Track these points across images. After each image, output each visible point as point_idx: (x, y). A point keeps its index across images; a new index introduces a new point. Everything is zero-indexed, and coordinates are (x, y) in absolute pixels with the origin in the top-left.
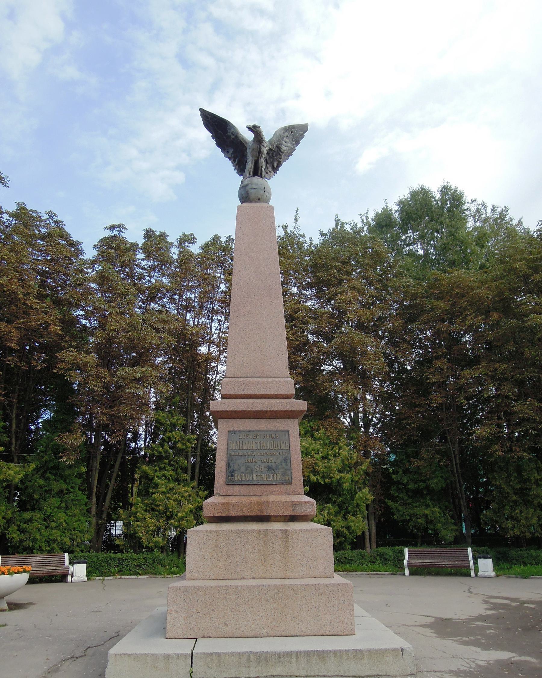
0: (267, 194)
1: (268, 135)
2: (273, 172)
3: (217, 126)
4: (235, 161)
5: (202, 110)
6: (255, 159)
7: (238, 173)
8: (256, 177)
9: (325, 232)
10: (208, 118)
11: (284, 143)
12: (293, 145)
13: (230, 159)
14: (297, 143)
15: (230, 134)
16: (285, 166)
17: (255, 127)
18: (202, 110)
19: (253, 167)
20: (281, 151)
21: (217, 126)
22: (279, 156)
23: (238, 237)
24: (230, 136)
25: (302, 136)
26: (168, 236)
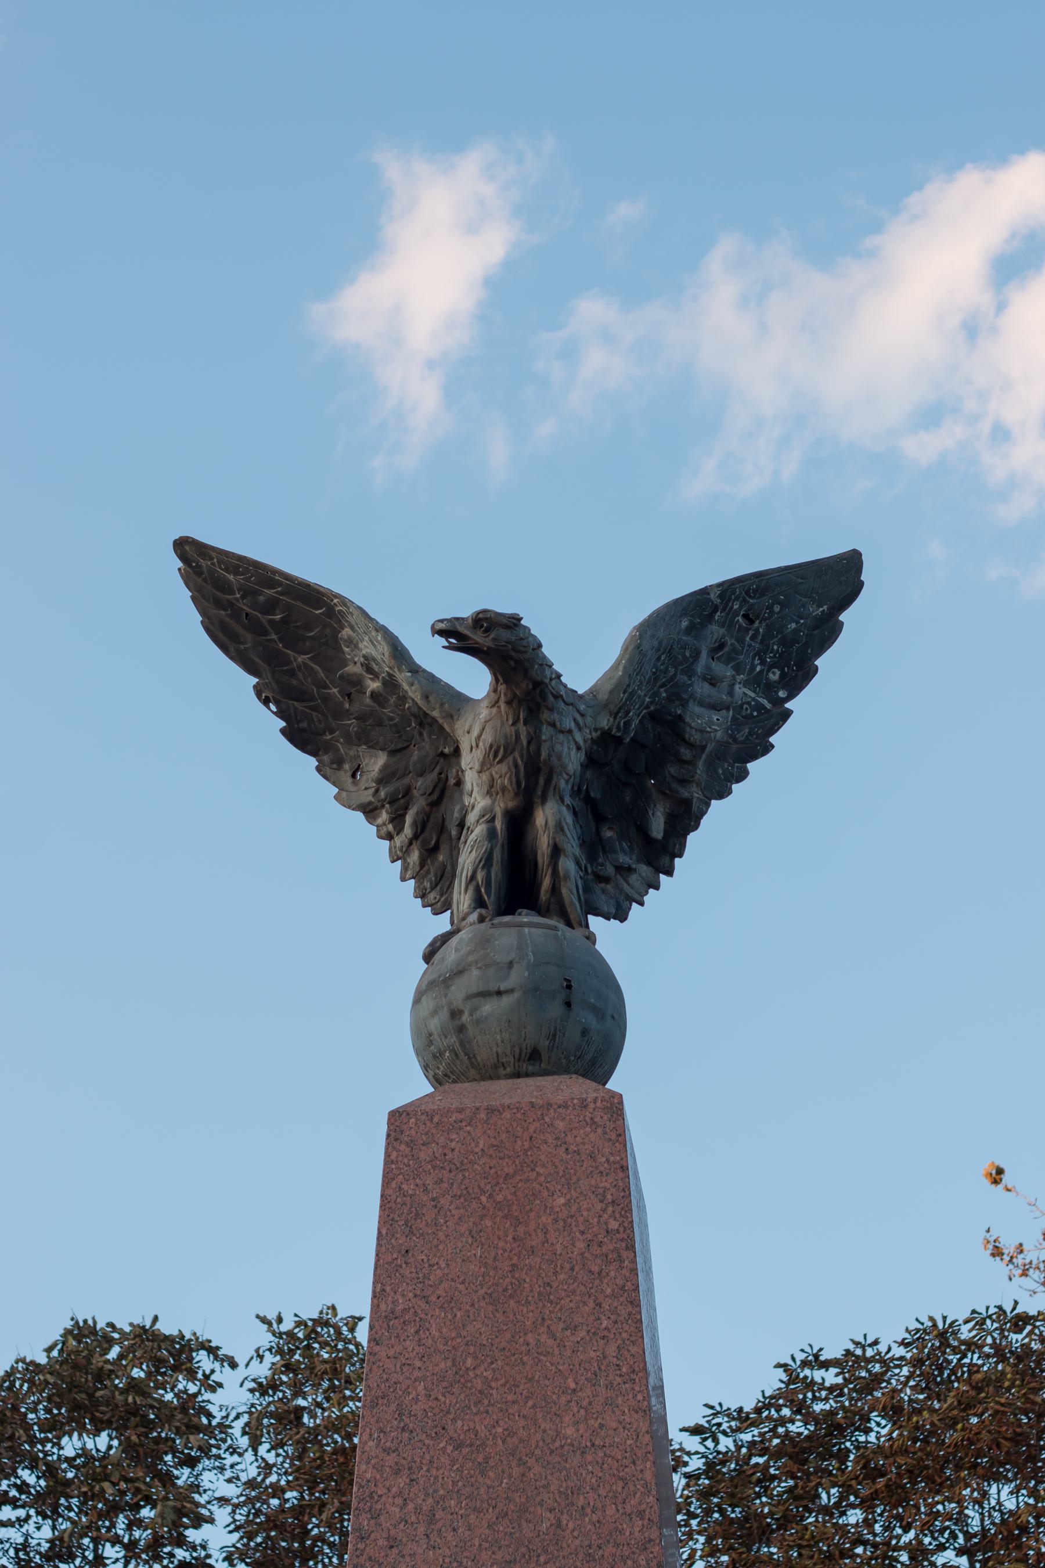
0: (590, 1019)
1: (585, 657)
2: (644, 869)
3: (274, 628)
4: (397, 820)
5: (188, 550)
6: (511, 804)
7: (421, 894)
8: (525, 917)
9: (910, 1328)
10: (225, 587)
11: (702, 689)
12: (769, 689)
13: (370, 811)
14: (799, 674)
15: (357, 669)
16: (725, 832)
17: (485, 621)
18: (188, 550)
19: (497, 855)
20: (681, 738)
21: (274, 628)
22: (673, 770)
23: (391, 1316)
24: (357, 683)
25: (826, 632)
26: (642, 904)
